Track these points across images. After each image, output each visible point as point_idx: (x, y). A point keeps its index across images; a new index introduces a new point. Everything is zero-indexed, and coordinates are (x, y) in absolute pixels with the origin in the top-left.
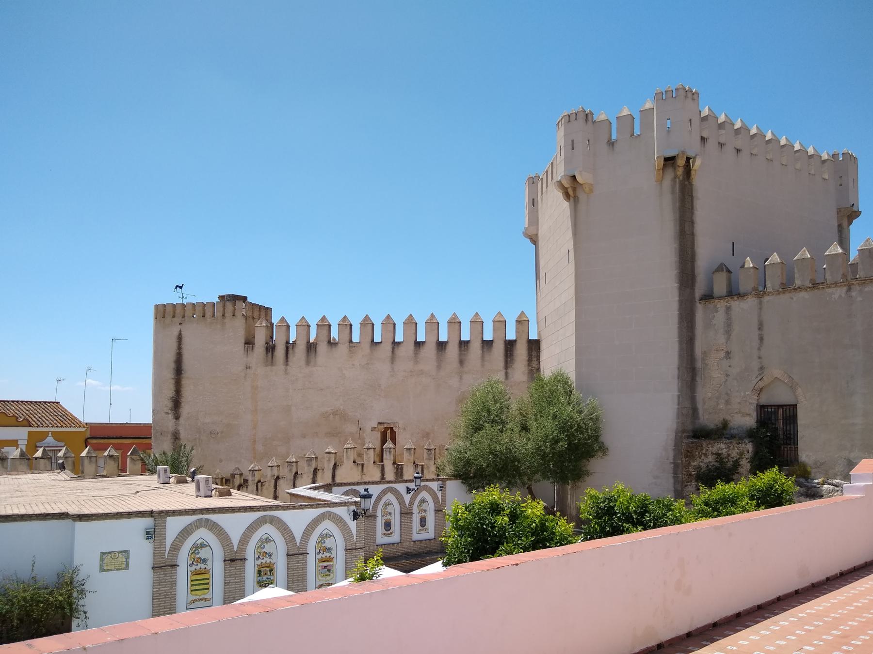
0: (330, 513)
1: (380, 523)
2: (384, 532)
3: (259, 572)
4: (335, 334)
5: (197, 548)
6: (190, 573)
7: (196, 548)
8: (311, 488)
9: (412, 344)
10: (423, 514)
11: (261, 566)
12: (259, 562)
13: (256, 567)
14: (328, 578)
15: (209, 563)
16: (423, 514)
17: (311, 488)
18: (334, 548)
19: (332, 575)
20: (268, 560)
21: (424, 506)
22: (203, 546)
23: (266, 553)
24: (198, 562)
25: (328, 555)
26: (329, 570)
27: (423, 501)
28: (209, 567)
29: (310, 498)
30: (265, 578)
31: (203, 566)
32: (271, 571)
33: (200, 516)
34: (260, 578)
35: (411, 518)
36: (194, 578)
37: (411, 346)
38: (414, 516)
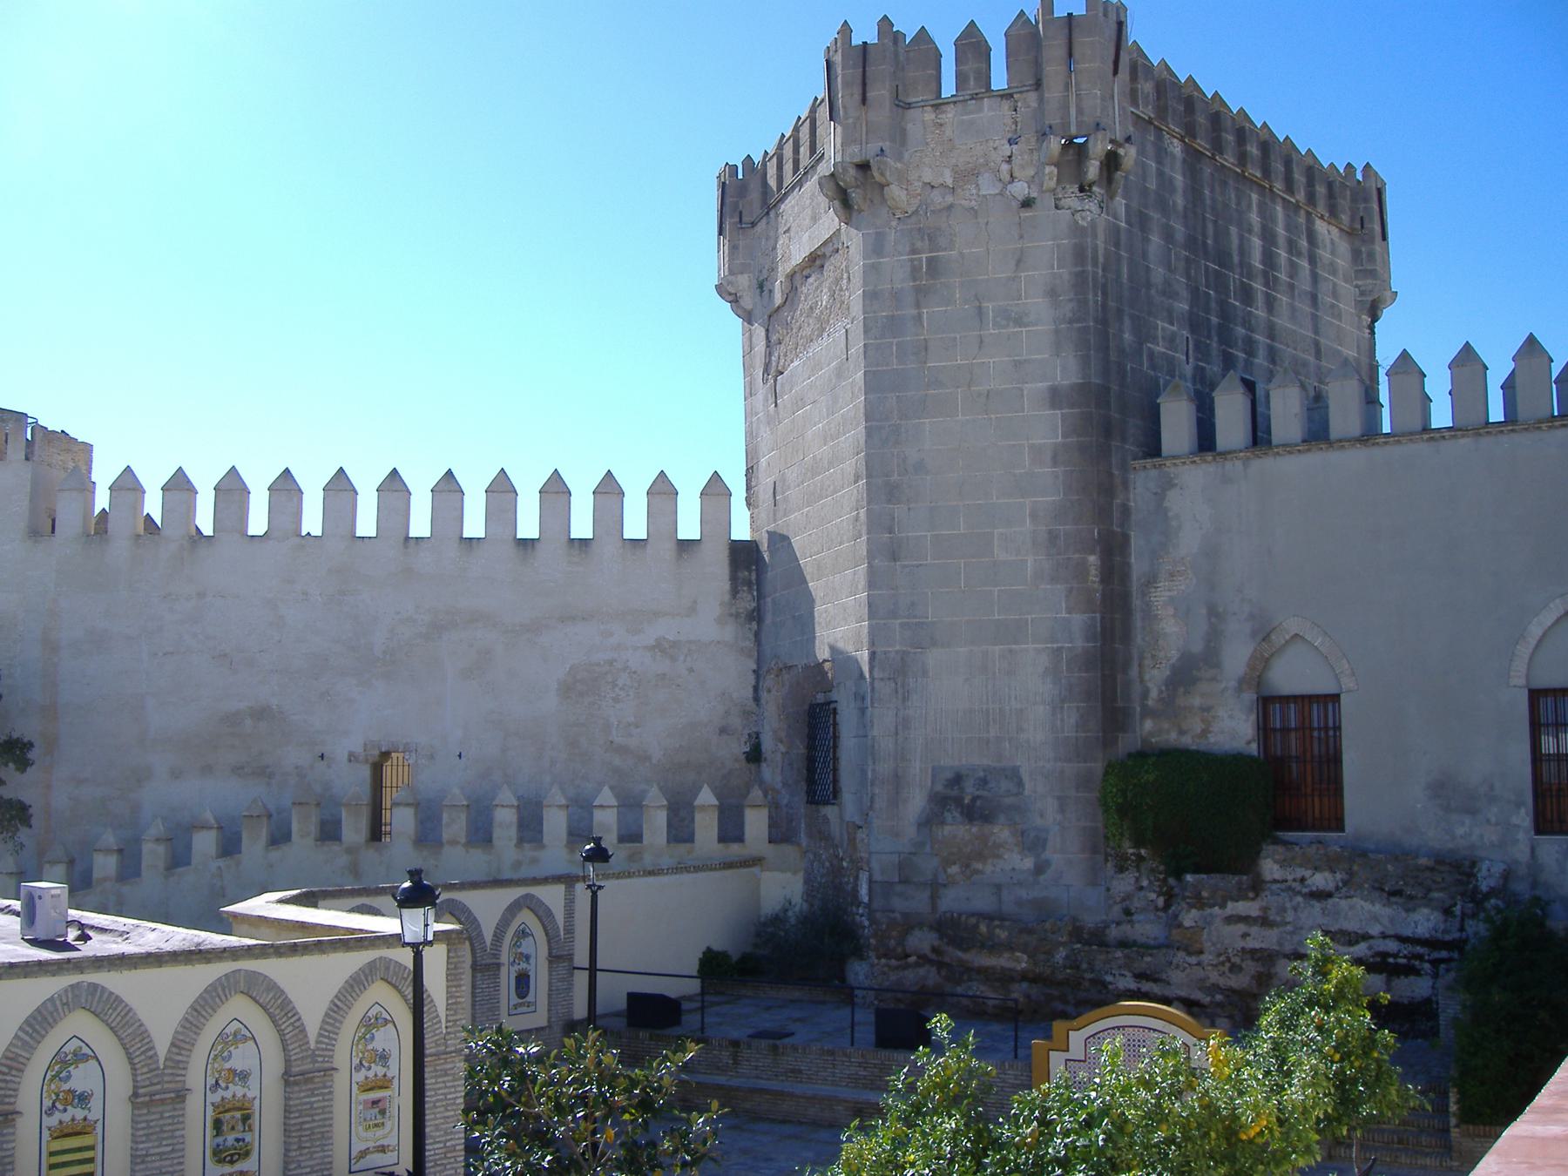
0: (253, 976)
1: (507, 978)
2: (515, 1000)
3: (218, 1124)
4: (153, 506)
5: (65, 1063)
6: (46, 1133)
7: (64, 1062)
8: (281, 901)
9: (671, 545)
10: (524, 965)
11: (222, 1108)
12: (215, 1098)
13: (210, 1109)
14: (380, 1132)
15: (95, 1104)
16: (524, 965)
17: (281, 901)
18: (395, 1053)
19: (388, 1124)
20: (79, 1114)
21: (527, 946)
22: (80, 1057)
23: (232, 1071)
24: (66, 1103)
25: (380, 1071)
26: (383, 1112)
27: (523, 933)
28: (95, 1114)
29: (303, 926)
30: (230, 1138)
31: (79, 1114)
32: (246, 1118)
33: (74, 979)
34: (220, 1140)
35: (497, 976)
36: (58, 1145)
37: (668, 550)
38: (504, 970)
